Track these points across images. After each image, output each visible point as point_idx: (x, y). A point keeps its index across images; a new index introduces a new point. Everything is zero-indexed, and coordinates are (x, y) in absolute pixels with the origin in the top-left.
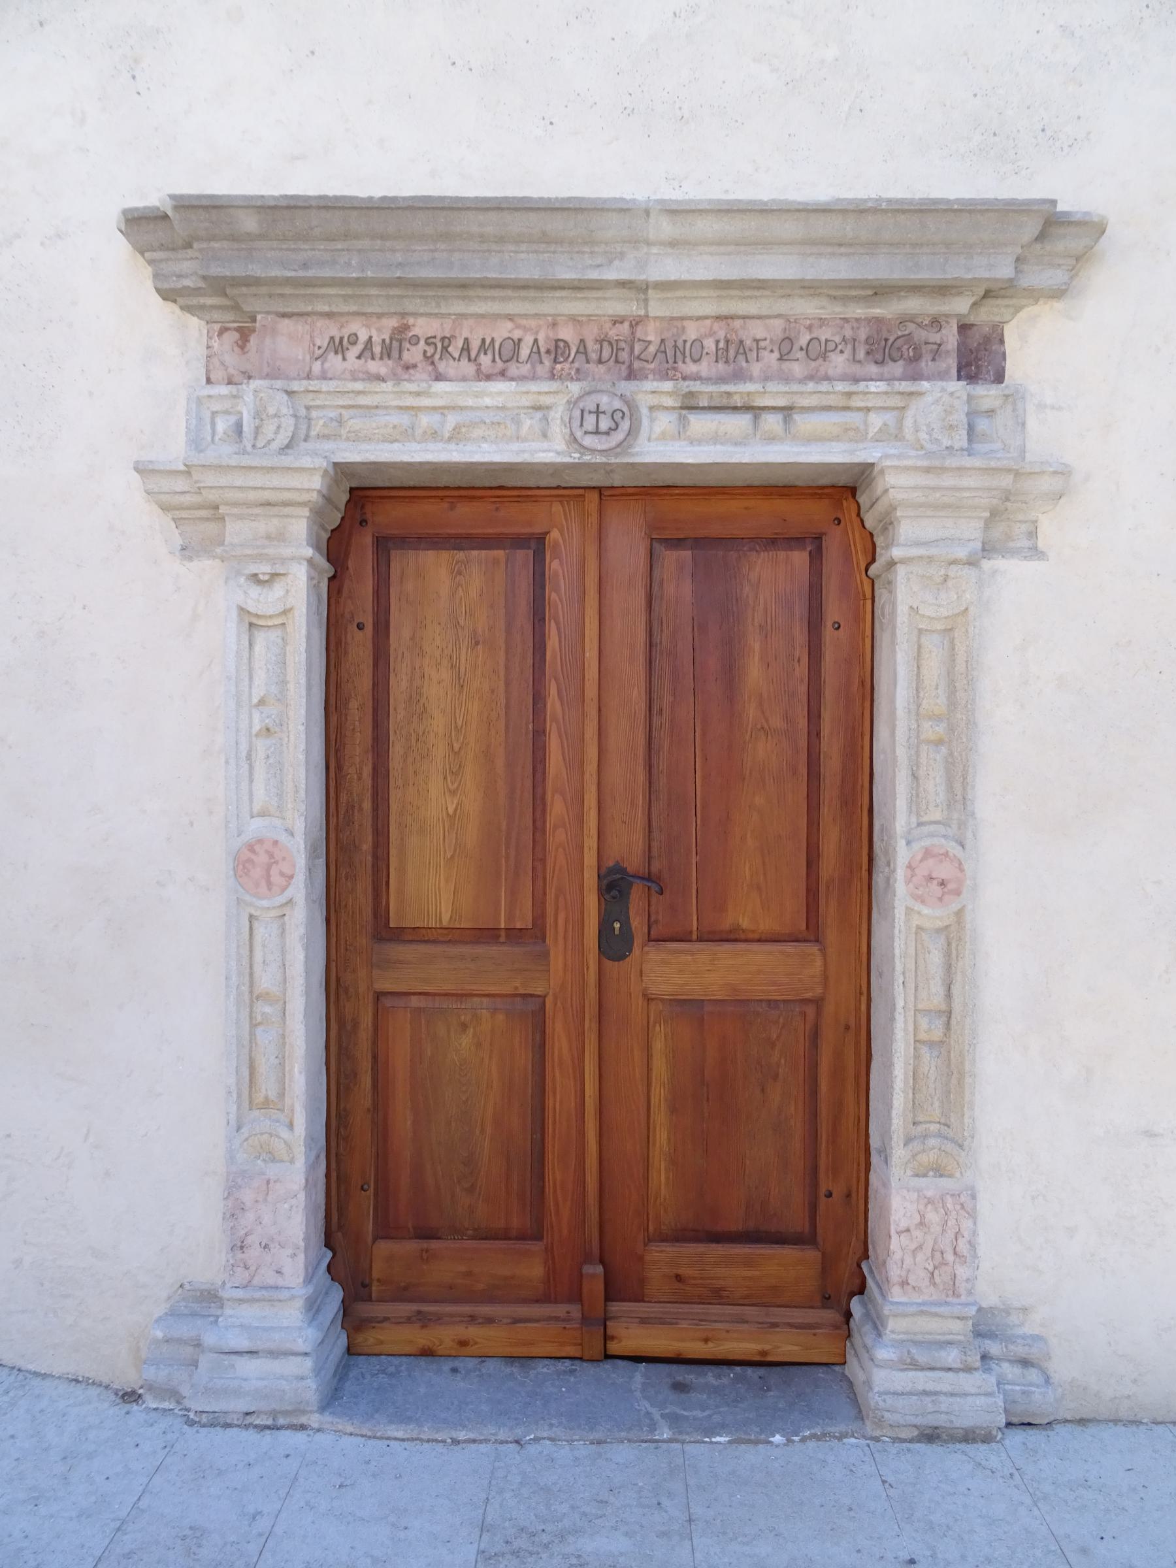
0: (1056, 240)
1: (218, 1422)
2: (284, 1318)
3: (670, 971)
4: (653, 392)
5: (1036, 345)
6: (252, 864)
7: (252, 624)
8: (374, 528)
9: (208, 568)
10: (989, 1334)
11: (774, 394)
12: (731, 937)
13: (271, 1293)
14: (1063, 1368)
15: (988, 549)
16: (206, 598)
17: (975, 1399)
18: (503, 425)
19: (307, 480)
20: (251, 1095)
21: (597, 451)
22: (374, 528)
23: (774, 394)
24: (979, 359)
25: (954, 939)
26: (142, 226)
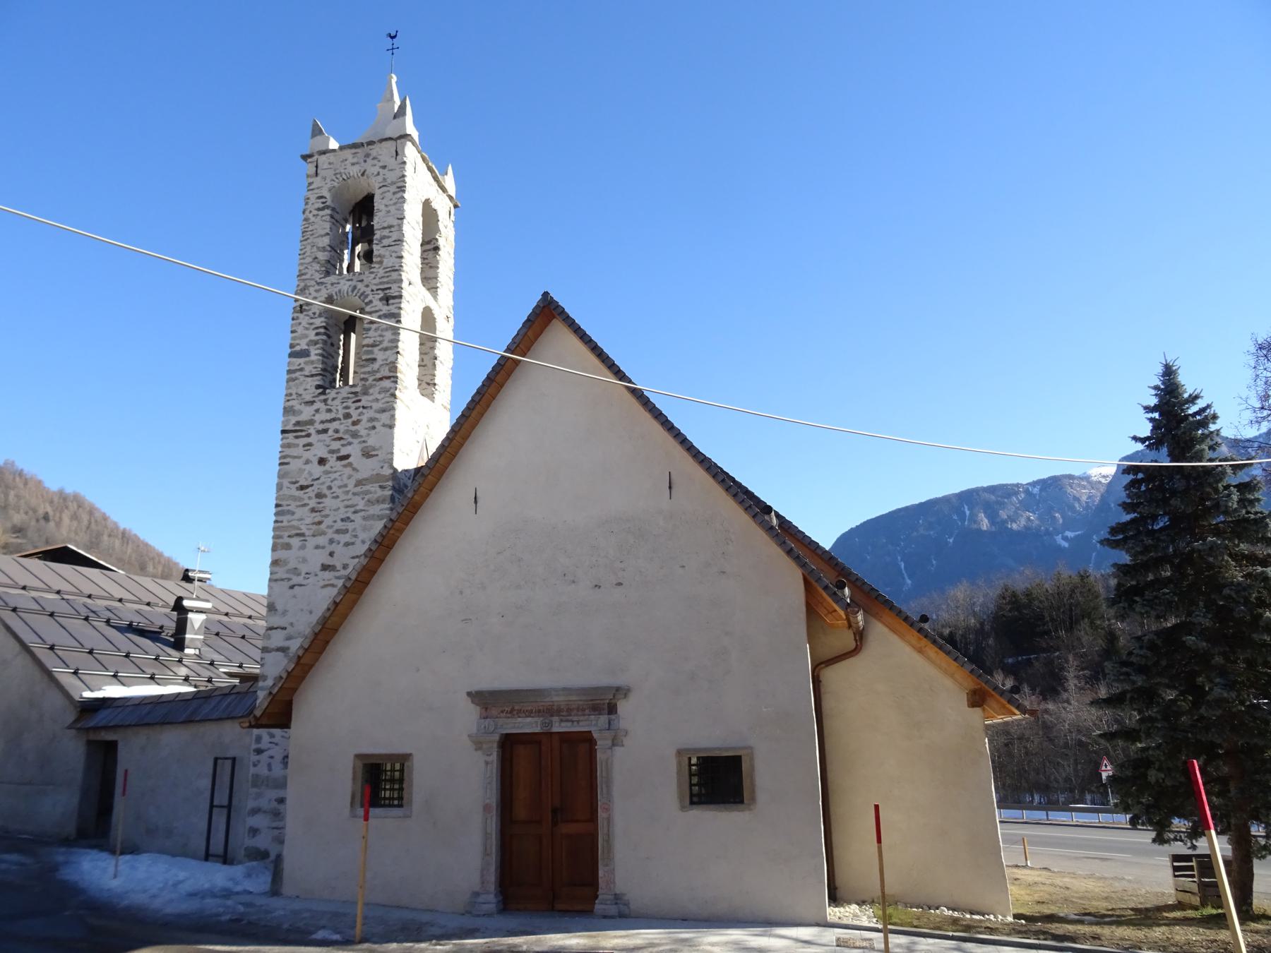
0: (621, 692)
1: (478, 916)
2: (490, 900)
3: (567, 829)
4: (555, 719)
5: (623, 707)
6: (486, 808)
7: (487, 763)
8: (509, 744)
9: (479, 753)
10: (617, 898)
11: (575, 718)
12: (577, 821)
13: (488, 893)
14: (632, 907)
15: (614, 745)
16: (479, 758)
17: (613, 910)
18: (529, 725)
19: (496, 737)
20: (486, 853)
21: (545, 730)
22: (509, 744)
23: (575, 718)
24: (612, 709)
25: (609, 820)
26: (469, 694)
